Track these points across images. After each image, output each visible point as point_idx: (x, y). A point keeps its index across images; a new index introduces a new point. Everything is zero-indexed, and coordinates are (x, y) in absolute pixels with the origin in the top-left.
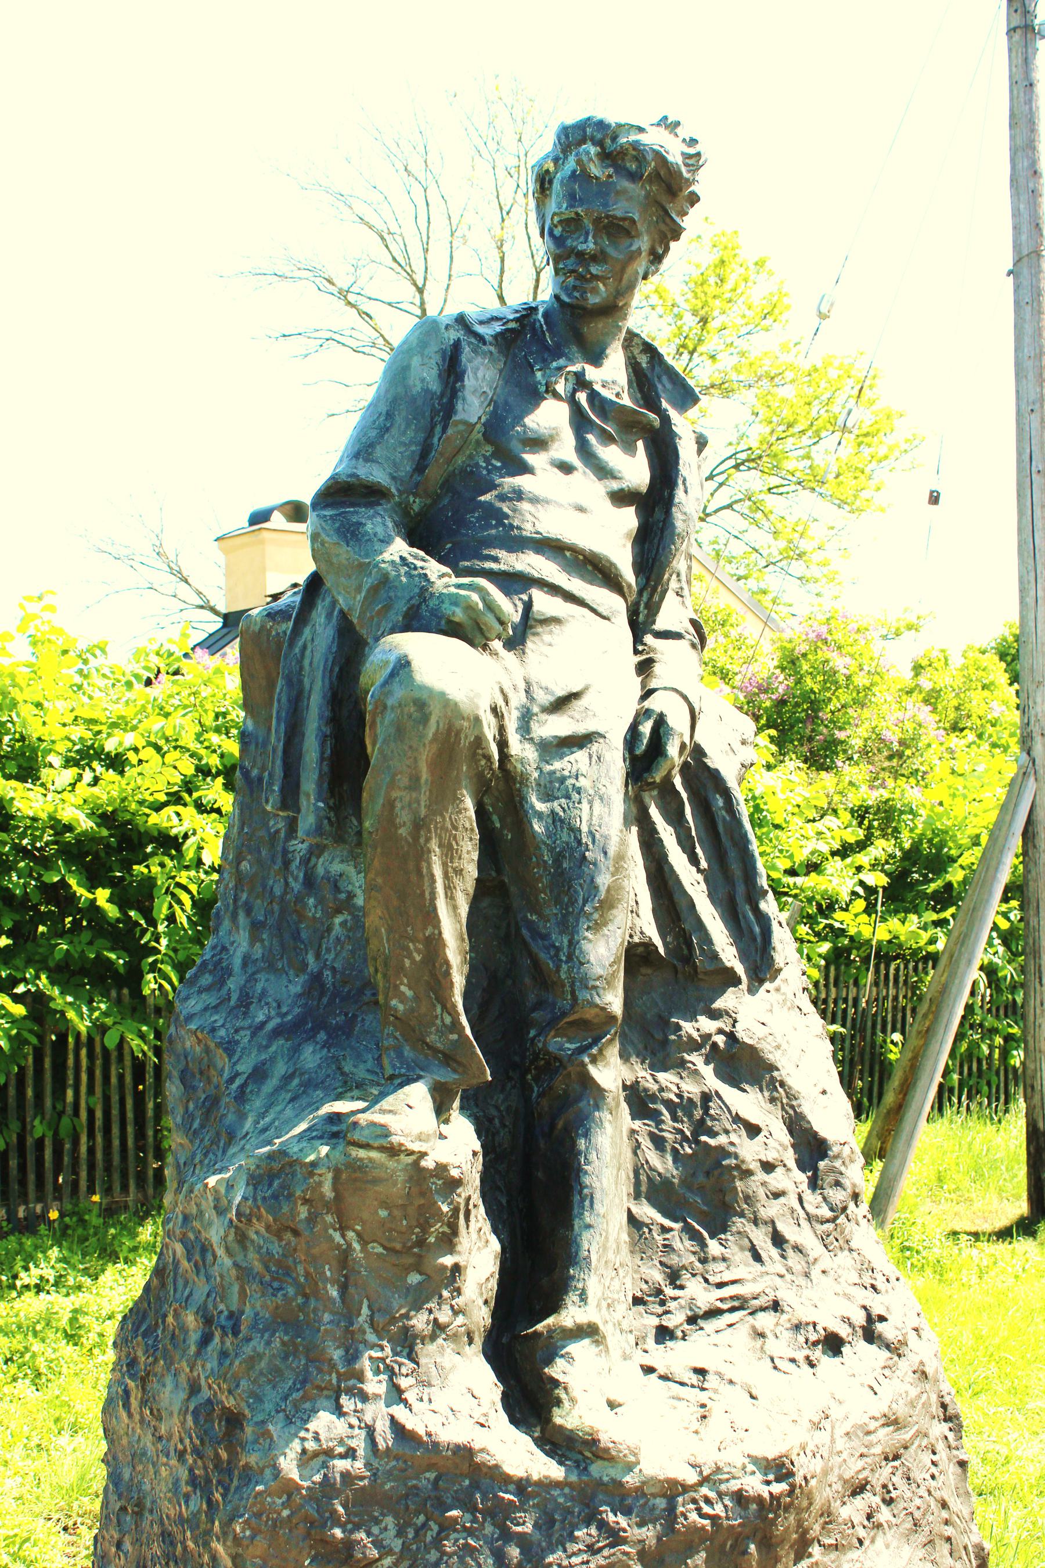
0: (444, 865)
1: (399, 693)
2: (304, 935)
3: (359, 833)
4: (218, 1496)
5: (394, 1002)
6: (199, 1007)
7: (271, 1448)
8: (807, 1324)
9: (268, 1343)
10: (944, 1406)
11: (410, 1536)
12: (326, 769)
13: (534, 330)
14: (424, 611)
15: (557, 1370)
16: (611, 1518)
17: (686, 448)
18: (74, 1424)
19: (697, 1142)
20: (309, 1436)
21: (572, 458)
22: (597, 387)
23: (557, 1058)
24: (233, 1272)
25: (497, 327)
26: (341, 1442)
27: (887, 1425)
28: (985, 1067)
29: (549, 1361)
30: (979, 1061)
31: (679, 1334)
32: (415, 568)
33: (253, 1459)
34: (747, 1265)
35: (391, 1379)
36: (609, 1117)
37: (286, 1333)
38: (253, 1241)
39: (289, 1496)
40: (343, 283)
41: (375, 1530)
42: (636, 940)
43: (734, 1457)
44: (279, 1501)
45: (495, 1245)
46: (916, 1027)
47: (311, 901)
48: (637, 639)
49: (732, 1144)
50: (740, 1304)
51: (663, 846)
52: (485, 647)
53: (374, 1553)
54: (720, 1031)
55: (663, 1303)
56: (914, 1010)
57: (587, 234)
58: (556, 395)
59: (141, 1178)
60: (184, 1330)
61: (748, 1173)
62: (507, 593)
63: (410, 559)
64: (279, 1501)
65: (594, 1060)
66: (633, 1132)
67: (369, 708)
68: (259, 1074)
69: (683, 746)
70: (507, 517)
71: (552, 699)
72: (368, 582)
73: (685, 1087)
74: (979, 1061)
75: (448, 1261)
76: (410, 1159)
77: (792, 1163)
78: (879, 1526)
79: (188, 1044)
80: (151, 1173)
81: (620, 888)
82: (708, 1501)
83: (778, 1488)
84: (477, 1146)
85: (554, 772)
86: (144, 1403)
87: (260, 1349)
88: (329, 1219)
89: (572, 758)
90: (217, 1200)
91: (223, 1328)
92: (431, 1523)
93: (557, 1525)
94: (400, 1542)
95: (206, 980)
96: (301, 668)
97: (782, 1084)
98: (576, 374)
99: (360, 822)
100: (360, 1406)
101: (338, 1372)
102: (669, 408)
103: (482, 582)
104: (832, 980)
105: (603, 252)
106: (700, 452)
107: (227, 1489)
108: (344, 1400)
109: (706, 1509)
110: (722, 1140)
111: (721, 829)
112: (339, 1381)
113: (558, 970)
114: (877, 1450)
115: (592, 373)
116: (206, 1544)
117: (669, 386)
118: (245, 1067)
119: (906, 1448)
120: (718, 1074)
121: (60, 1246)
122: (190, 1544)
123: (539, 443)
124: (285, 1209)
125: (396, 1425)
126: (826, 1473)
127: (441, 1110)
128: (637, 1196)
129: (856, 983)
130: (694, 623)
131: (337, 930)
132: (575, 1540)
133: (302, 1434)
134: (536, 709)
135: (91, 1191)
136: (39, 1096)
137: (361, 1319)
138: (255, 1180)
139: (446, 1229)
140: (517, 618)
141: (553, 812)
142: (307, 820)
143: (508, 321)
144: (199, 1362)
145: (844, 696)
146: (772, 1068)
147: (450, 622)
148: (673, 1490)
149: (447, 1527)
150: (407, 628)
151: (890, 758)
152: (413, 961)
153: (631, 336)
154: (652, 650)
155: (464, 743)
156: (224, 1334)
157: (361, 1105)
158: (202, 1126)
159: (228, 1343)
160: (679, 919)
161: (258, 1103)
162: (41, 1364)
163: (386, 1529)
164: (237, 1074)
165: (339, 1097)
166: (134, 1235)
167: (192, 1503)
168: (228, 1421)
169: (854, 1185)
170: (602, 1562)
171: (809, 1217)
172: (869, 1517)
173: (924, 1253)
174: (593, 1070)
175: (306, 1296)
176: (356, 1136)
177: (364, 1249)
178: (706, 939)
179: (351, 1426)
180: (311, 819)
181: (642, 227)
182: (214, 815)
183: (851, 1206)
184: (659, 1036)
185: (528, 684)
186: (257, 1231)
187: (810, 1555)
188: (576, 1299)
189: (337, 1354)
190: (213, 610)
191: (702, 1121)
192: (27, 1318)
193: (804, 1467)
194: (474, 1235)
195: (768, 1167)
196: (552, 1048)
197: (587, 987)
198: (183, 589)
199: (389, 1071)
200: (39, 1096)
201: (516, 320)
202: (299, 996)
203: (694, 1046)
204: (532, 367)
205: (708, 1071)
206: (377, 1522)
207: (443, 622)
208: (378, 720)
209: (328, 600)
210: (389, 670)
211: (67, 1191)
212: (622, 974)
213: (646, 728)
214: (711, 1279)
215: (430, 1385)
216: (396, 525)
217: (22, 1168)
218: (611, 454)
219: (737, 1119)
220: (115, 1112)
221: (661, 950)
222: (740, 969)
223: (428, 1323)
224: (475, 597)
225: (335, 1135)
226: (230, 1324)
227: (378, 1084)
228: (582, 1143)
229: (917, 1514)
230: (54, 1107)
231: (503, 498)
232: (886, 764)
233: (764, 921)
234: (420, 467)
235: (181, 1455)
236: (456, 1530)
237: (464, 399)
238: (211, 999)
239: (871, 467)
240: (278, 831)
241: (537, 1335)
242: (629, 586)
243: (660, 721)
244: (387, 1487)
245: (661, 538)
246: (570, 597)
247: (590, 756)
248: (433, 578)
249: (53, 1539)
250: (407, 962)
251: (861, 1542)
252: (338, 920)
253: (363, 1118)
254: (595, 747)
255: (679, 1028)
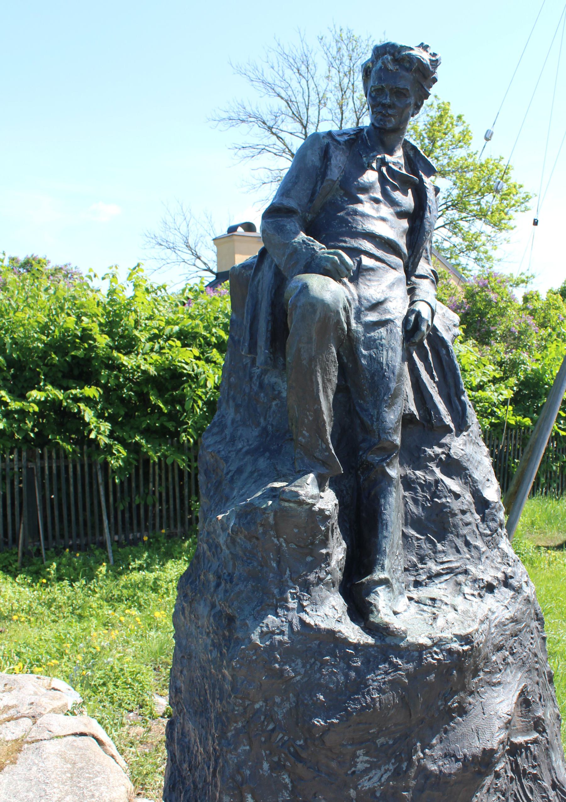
0: (323, 377)
1: (303, 300)
2: (259, 410)
3: (284, 365)
4: (224, 650)
5: (300, 438)
6: (212, 442)
7: (248, 631)
8: (480, 579)
9: (246, 586)
10: (537, 614)
11: (308, 667)
12: (269, 335)
13: (362, 139)
14: (313, 265)
15: (371, 598)
16: (395, 660)
17: (430, 194)
18: (157, 626)
19: (433, 501)
20: (264, 625)
21: (379, 196)
22: (391, 165)
23: (371, 464)
24: (230, 556)
25: (346, 138)
26: (278, 628)
27: (511, 622)
28: (553, 475)
29: (368, 595)
30: (551, 473)
31: (424, 583)
32: (309, 245)
33: (240, 635)
34: (453, 554)
35: (299, 602)
36: (394, 490)
37: (254, 582)
38: (238, 543)
39: (256, 650)
40: (270, 123)
41: (293, 665)
42: (407, 412)
43: (447, 635)
44: (251, 653)
45: (344, 545)
46: (524, 457)
47: (262, 395)
48: (408, 278)
49: (448, 502)
50: (450, 571)
51: (419, 371)
52: (340, 281)
53: (293, 674)
54: (443, 453)
55: (417, 570)
56: (523, 450)
57: (387, 95)
58: (373, 169)
59: (183, 524)
60: (208, 581)
61: (455, 515)
62: (351, 257)
63: (307, 241)
64: (251, 653)
65: (388, 465)
66: (404, 497)
67: (289, 307)
68: (240, 471)
69: (428, 326)
70: (350, 223)
71: (370, 304)
72: (288, 251)
73: (427, 477)
74: (551, 473)
75: (324, 551)
76: (308, 507)
77: (474, 511)
78: (508, 664)
79: (208, 458)
80: (187, 520)
81: (400, 389)
82: (436, 653)
83: (466, 648)
84: (337, 501)
85: (371, 337)
86: (191, 612)
87: (242, 588)
88: (272, 533)
89: (379, 331)
90: (222, 525)
91: (226, 580)
92: (317, 662)
93: (371, 663)
94: (304, 670)
95: (215, 430)
96: (257, 291)
97: (470, 476)
98: (381, 159)
99: (285, 358)
100: (286, 613)
101: (276, 599)
102: (423, 175)
103: (340, 252)
104: (487, 438)
105: (394, 104)
106: (436, 195)
107: (229, 648)
108: (279, 610)
109: (436, 656)
110: (444, 500)
111: (444, 364)
112: (277, 603)
113: (372, 424)
114: (508, 633)
115: (388, 158)
116: (220, 671)
117: (422, 165)
118: (233, 468)
119: (520, 632)
120: (442, 472)
121: (148, 551)
122: (213, 671)
123: (365, 189)
124: (253, 528)
125: (302, 621)
126: (486, 641)
127: (321, 488)
128: (406, 524)
129: (498, 439)
130: (433, 271)
131: (274, 407)
132: (379, 669)
133: (261, 625)
134: (363, 309)
135: (161, 528)
136: (137, 487)
137: (286, 576)
138: (239, 516)
139: (323, 538)
140: (354, 268)
141: (370, 355)
142: (261, 358)
143: (351, 135)
144: (215, 595)
145: (494, 311)
146: (466, 469)
147: (324, 269)
148: (422, 648)
149: (324, 664)
150: (306, 272)
151: (514, 339)
152: (309, 420)
153: (406, 142)
154: (414, 283)
155: (332, 323)
156: (226, 582)
157: (285, 484)
158: (214, 494)
159: (228, 587)
160: (426, 403)
161: (239, 484)
162: (142, 601)
163: (297, 664)
164: (230, 471)
165: (276, 481)
166: (180, 547)
167: (213, 654)
168: (229, 619)
169: (500, 520)
170: (390, 678)
171: (481, 534)
172: (504, 660)
173: (525, 555)
174: (388, 470)
175: (262, 566)
176: (284, 497)
177: (287, 546)
178: (438, 412)
179: (282, 622)
180: (262, 358)
181: (411, 93)
182: (213, 364)
183: (500, 530)
184: (416, 455)
185: (359, 297)
186: (240, 539)
187: (479, 676)
188: (380, 568)
189: (276, 591)
190: (211, 271)
191: (435, 492)
192: (135, 581)
193: (479, 639)
194: (335, 541)
195: (464, 512)
196: (369, 459)
197: (385, 433)
198: (198, 262)
199: (298, 469)
200: (137, 487)
201: (354, 134)
202: (257, 437)
203: (431, 459)
204: (361, 156)
205: (437, 471)
206: (294, 662)
207: (322, 269)
208: (293, 312)
209: (269, 260)
210: (298, 290)
211: (151, 527)
212: (400, 427)
213: (412, 318)
214: (438, 560)
215: (316, 604)
216: (300, 226)
217: (131, 518)
218: (397, 195)
219: (450, 491)
220: (171, 493)
221: (418, 418)
222: (452, 426)
223: (315, 578)
224: (336, 258)
225: (274, 497)
226: (228, 578)
227: (292, 475)
228: (383, 501)
229: (524, 659)
230: (144, 491)
231: (348, 214)
232: (513, 342)
233: (463, 404)
234: (311, 201)
235: (208, 634)
236: (328, 665)
237: (331, 170)
238: (218, 438)
239: (507, 209)
240: (247, 364)
241: (362, 583)
242: (405, 254)
243: (418, 314)
244: (298, 647)
245: (419, 233)
246: (378, 259)
247: (387, 330)
248: (317, 249)
249: (150, 673)
250: (306, 421)
251: (500, 670)
252: (274, 403)
253: (287, 489)
254: (389, 326)
255: (425, 451)
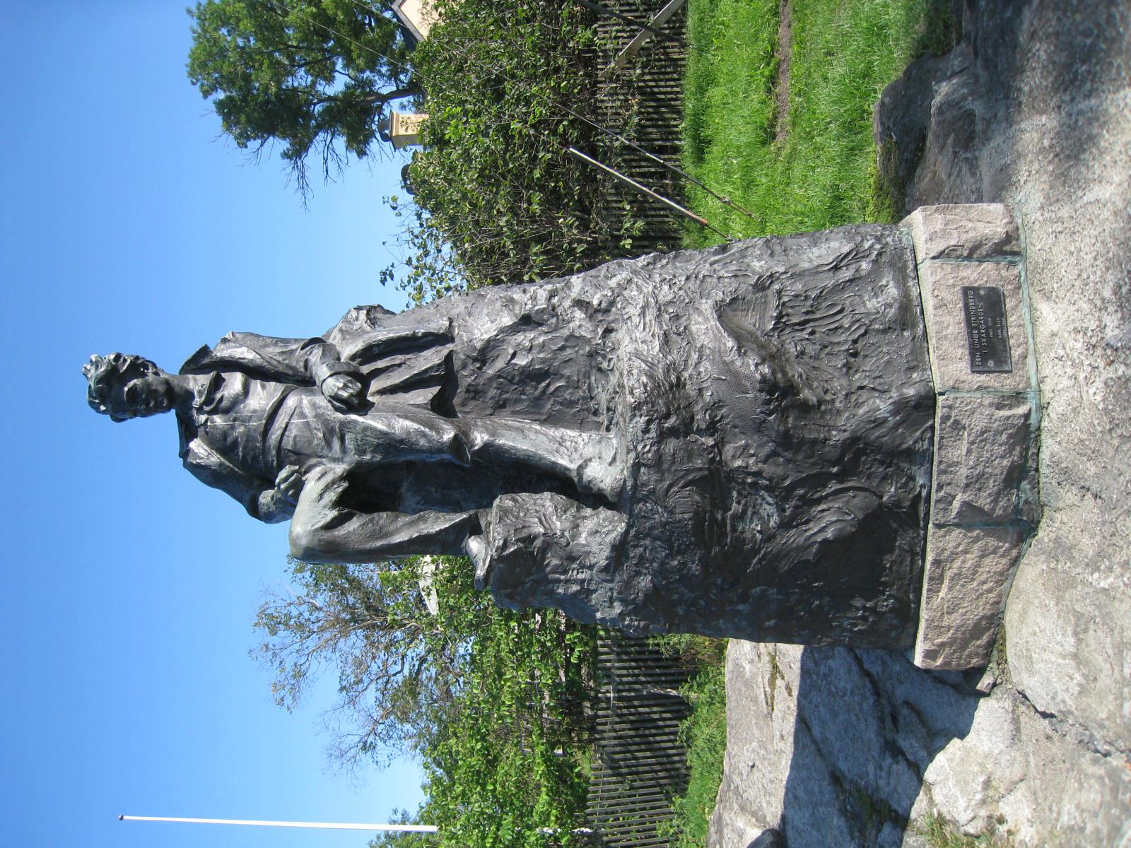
29: (591, 489)
76: (494, 563)
82: (645, 447)
109: (648, 448)
